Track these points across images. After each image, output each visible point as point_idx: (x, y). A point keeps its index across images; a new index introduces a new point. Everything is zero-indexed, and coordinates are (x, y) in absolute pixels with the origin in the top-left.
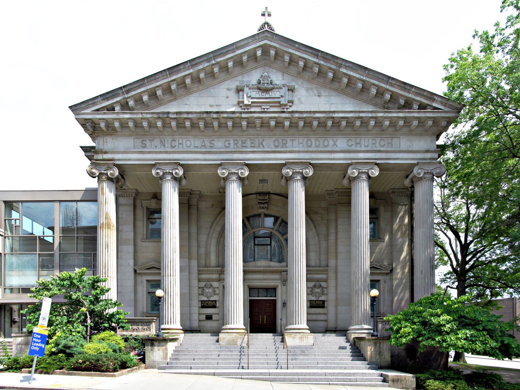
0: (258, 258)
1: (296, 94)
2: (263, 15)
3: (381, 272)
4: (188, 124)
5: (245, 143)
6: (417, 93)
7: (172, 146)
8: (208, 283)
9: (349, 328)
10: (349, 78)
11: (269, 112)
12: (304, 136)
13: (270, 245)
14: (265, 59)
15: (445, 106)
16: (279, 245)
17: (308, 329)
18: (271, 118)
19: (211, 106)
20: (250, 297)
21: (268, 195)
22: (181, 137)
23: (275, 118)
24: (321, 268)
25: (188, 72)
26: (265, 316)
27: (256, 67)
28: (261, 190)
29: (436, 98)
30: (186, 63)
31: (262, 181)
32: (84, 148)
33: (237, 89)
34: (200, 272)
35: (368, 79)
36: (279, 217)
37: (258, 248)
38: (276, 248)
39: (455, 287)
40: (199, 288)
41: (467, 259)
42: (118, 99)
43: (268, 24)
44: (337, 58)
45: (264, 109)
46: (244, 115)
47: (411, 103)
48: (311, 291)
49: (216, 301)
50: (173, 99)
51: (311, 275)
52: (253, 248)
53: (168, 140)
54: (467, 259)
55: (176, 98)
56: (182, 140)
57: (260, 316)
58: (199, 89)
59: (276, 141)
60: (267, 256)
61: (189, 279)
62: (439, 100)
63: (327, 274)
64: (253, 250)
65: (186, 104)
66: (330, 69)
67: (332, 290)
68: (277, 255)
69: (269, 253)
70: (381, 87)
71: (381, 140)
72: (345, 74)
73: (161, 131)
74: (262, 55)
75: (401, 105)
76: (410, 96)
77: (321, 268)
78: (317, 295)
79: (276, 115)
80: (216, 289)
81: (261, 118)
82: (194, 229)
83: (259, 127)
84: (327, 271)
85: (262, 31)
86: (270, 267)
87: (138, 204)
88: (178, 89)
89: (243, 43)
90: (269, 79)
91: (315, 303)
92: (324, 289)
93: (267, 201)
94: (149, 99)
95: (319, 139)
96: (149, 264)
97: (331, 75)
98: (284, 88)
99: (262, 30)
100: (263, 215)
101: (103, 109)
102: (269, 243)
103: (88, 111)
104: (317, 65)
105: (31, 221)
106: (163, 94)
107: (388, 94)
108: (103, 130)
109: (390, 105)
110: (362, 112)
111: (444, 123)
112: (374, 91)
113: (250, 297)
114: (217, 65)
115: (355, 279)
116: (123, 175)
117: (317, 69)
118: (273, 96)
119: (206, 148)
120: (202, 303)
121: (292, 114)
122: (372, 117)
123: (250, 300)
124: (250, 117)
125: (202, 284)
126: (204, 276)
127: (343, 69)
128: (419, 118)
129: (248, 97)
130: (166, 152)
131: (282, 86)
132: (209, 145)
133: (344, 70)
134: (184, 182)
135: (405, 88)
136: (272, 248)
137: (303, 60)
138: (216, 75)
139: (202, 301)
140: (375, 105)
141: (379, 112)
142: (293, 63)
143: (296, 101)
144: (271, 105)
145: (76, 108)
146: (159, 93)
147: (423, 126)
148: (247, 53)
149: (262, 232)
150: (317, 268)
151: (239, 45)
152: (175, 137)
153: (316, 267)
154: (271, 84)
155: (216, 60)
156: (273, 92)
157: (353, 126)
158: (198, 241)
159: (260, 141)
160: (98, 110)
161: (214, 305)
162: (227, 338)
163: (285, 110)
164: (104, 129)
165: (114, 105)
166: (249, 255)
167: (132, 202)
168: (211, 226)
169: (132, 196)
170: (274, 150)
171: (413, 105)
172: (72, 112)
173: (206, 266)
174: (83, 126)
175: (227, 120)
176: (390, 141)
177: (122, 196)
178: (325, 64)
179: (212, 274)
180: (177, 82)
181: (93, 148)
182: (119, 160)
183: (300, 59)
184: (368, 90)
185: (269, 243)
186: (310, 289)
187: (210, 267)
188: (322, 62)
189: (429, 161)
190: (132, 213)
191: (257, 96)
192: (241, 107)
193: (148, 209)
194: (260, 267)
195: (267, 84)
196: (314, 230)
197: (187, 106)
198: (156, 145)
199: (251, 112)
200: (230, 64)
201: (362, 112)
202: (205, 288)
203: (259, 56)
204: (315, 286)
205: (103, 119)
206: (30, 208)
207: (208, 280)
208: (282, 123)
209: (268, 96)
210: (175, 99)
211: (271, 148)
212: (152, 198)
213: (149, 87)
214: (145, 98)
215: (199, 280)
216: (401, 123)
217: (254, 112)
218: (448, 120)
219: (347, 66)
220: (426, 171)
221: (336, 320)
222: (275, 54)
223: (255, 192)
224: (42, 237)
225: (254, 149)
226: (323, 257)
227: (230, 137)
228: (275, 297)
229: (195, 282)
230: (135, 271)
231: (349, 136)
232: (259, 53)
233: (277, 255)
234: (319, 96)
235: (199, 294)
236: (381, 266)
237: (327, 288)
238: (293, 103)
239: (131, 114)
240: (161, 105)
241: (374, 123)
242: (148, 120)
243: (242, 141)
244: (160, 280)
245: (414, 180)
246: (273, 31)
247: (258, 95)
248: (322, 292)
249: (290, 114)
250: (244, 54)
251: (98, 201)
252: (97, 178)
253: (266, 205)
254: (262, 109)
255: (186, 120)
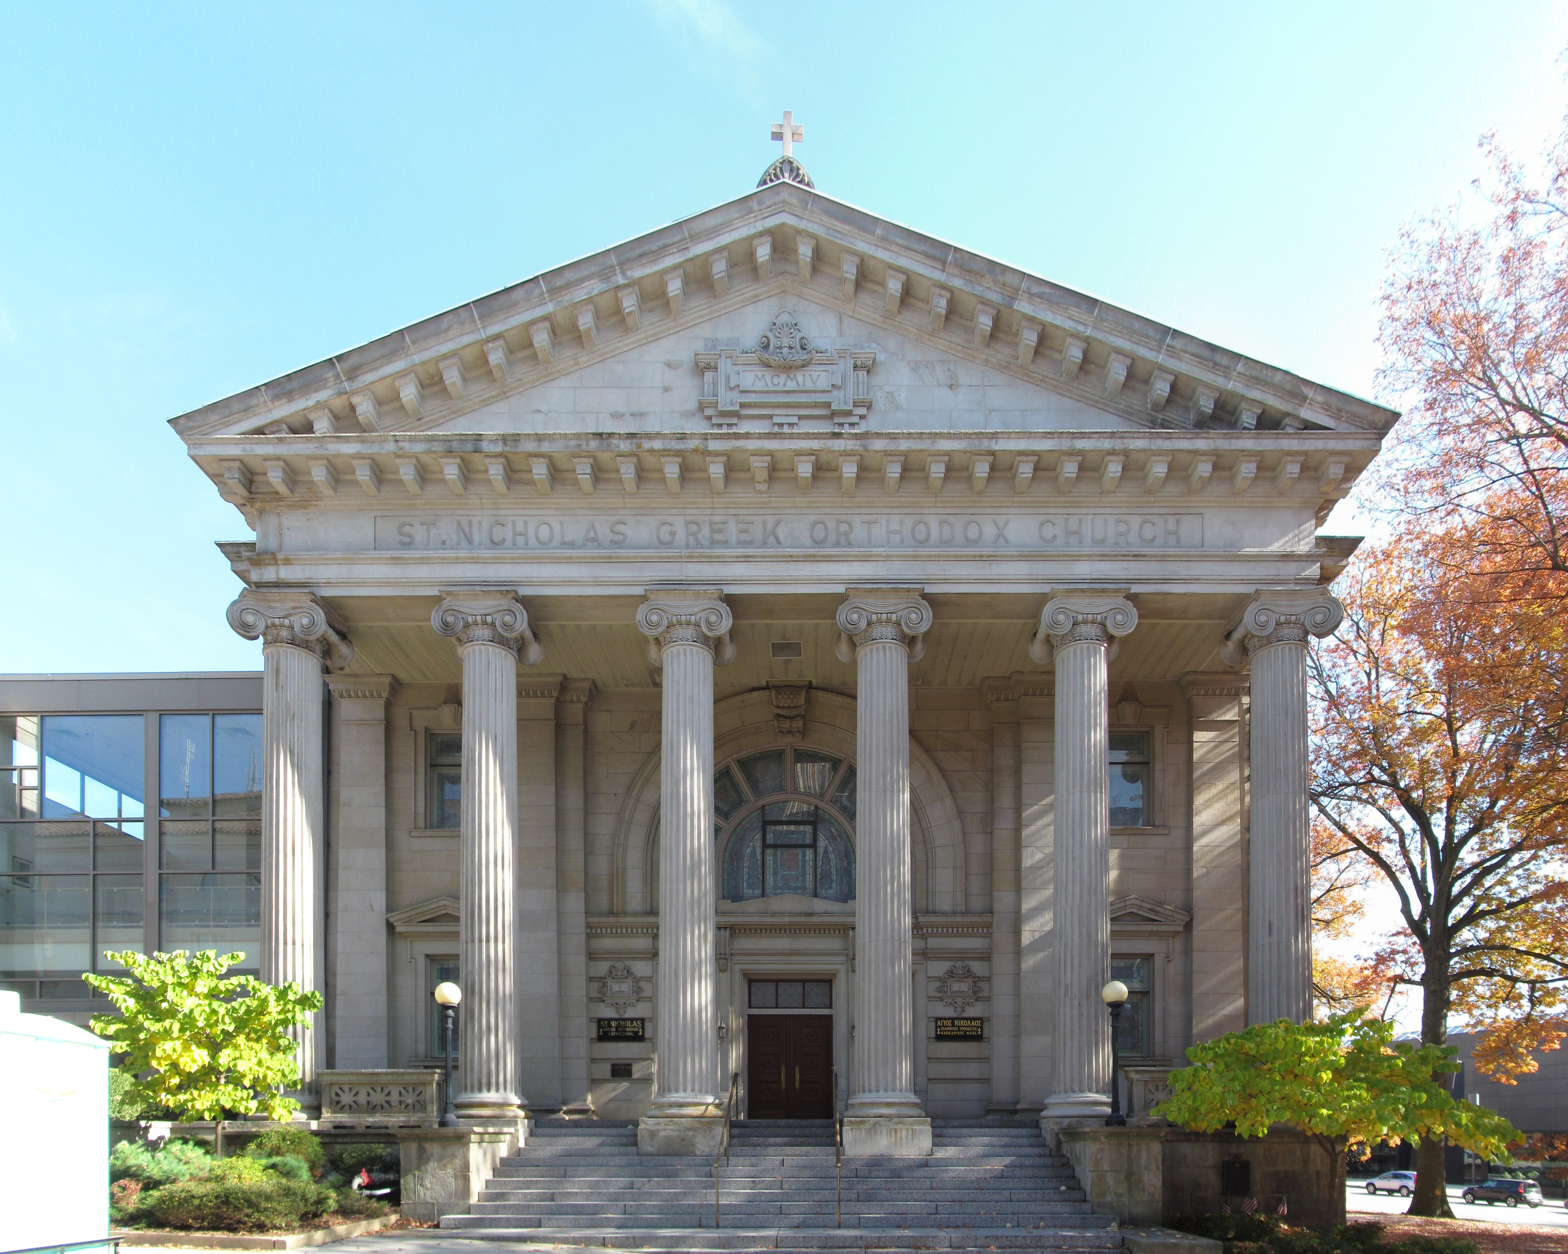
0: (775, 888)
1: (879, 379)
2: (778, 136)
3: (1155, 928)
4: (540, 470)
5: (720, 531)
6: (1252, 377)
7: (492, 541)
8: (619, 965)
9: (1046, 1101)
10: (1043, 330)
11: (791, 436)
12: (904, 511)
13: (814, 846)
14: (782, 273)
15: (1337, 418)
16: (842, 848)
17: (915, 1105)
18: (799, 453)
19: (616, 416)
20: (750, 1007)
21: (803, 694)
22: (520, 512)
23: (812, 452)
24: (969, 919)
25: (539, 312)
26: (797, 1070)
27: (756, 296)
28: (780, 677)
29: (1309, 392)
30: (532, 285)
31: (780, 648)
32: (229, 549)
33: (697, 365)
34: (592, 932)
35: (1099, 335)
36: (840, 761)
37: (775, 855)
38: (832, 856)
39: (1417, 978)
40: (591, 979)
41: (1456, 889)
42: (322, 396)
43: (791, 163)
44: (1005, 269)
45: (781, 425)
46: (714, 445)
47: (1235, 409)
48: (939, 990)
49: (643, 1020)
50: (498, 396)
51: (940, 940)
52: (759, 856)
53: (480, 523)
54: (1456, 889)
55: (504, 393)
56: (526, 523)
57: (783, 1069)
58: (577, 364)
59: (820, 527)
60: (804, 881)
61: (559, 953)
62: (1320, 398)
63: (989, 936)
64: (760, 863)
65: (539, 411)
66: (983, 303)
67: (1002, 986)
68: (834, 877)
69: (810, 871)
70: (1142, 359)
71: (1145, 522)
72: (1031, 319)
73: (459, 496)
74: (773, 259)
75: (1201, 414)
76: (1230, 386)
77: (969, 919)
78: (959, 1001)
79: (815, 445)
80: (643, 984)
81: (771, 454)
82: (574, 798)
83: (765, 481)
84: (989, 925)
85: (770, 185)
86: (811, 914)
87: (401, 721)
88: (510, 363)
89: (711, 222)
90: (795, 333)
91: (953, 1024)
92: (980, 984)
93: (801, 711)
94: (423, 398)
95: (952, 519)
96: (435, 905)
97: (985, 322)
98: (842, 362)
99: (771, 181)
100: (789, 756)
101: (274, 428)
102: (808, 841)
103: (231, 433)
104: (943, 292)
105: (78, 774)
106: (464, 379)
107: (1164, 380)
108: (277, 493)
109: (1172, 415)
110: (1082, 435)
111: (1335, 470)
112: (1118, 371)
113: (750, 1007)
114: (631, 289)
115: (1062, 949)
116: (344, 629)
117: (943, 303)
118: (809, 386)
119: (600, 546)
120: (599, 1027)
121: (864, 442)
122: (1113, 452)
123: (749, 1016)
124: (734, 450)
125: (602, 968)
126: (608, 943)
127: (1023, 304)
128: (1260, 453)
129: (731, 389)
130: (476, 561)
131: (836, 356)
132: (611, 536)
133: (1027, 305)
134: (534, 652)
135: (1216, 364)
136: (820, 857)
137: (900, 275)
138: (629, 321)
139: (600, 1020)
140: (1127, 414)
141: (1133, 436)
142: (871, 286)
143: (881, 404)
144: (803, 412)
145: (191, 424)
146: (452, 377)
147: (1273, 479)
148: (725, 254)
149: (794, 807)
150: (959, 919)
151: (697, 226)
152: (503, 512)
153: (954, 913)
154: (803, 348)
155: (629, 274)
156: (807, 374)
157: (1056, 478)
158: (586, 833)
159: (770, 526)
160: (260, 431)
161: (636, 1033)
162: (662, 1134)
163: (846, 430)
164: (282, 489)
165: (311, 417)
166: (746, 877)
167: (380, 714)
168: (630, 788)
169: (380, 696)
170: (811, 551)
171: (1241, 413)
172: (178, 437)
173: (611, 913)
174: (215, 477)
175: (663, 459)
176: (1171, 527)
177: (350, 696)
178: (968, 289)
179: (632, 935)
180: (507, 343)
181: (251, 546)
182: (328, 584)
183: (891, 272)
184: (1104, 367)
185: (808, 841)
186: (938, 984)
187: (625, 913)
188: (957, 283)
189: (1292, 587)
190: (382, 748)
191: (760, 386)
192: (709, 418)
193: (430, 735)
194: (781, 914)
195: (791, 348)
196: (949, 801)
197: (539, 417)
198: (444, 537)
199: (737, 436)
200: (674, 287)
201: (1082, 435)
202: (609, 982)
203: (762, 263)
204: (951, 974)
205: (278, 458)
206: (69, 733)
207: (620, 955)
208: (836, 470)
209: (791, 385)
210: (504, 395)
211: (802, 547)
212: (445, 703)
213: (417, 359)
214: (409, 393)
215: (592, 956)
216: (1204, 469)
217: (747, 436)
218: (1346, 459)
219: (1034, 295)
220: (1283, 619)
221: (1017, 1079)
222: (813, 258)
223: (764, 684)
224: (115, 825)
225: (750, 551)
226: (976, 885)
227: (674, 511)
228: (830, 1007)
229: (577, 962)
230: (390, 927)
231: (1046, 511)
232: (763, 252)
233: (834, 877)
234: (951, 386)
235: (591, 1000)
236: (1157, 913)
237: (989, 979)
238: (869, 407)
239: (363, 441)
240: (460, 413)
241: (1120, 469)
242: (418, 460)
243: (712, 524)
244: (458, 956)
245: (1250, 645)
246: (808, 185)
247: (763, 383)
248: (975, 993)
249: (858, 442)
250: (716, 257)
251: (265, 712)
252: (261, 638)
253: (799, 724)
254: (774, 424)
255: (535, 460)
